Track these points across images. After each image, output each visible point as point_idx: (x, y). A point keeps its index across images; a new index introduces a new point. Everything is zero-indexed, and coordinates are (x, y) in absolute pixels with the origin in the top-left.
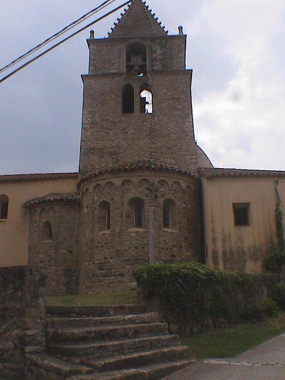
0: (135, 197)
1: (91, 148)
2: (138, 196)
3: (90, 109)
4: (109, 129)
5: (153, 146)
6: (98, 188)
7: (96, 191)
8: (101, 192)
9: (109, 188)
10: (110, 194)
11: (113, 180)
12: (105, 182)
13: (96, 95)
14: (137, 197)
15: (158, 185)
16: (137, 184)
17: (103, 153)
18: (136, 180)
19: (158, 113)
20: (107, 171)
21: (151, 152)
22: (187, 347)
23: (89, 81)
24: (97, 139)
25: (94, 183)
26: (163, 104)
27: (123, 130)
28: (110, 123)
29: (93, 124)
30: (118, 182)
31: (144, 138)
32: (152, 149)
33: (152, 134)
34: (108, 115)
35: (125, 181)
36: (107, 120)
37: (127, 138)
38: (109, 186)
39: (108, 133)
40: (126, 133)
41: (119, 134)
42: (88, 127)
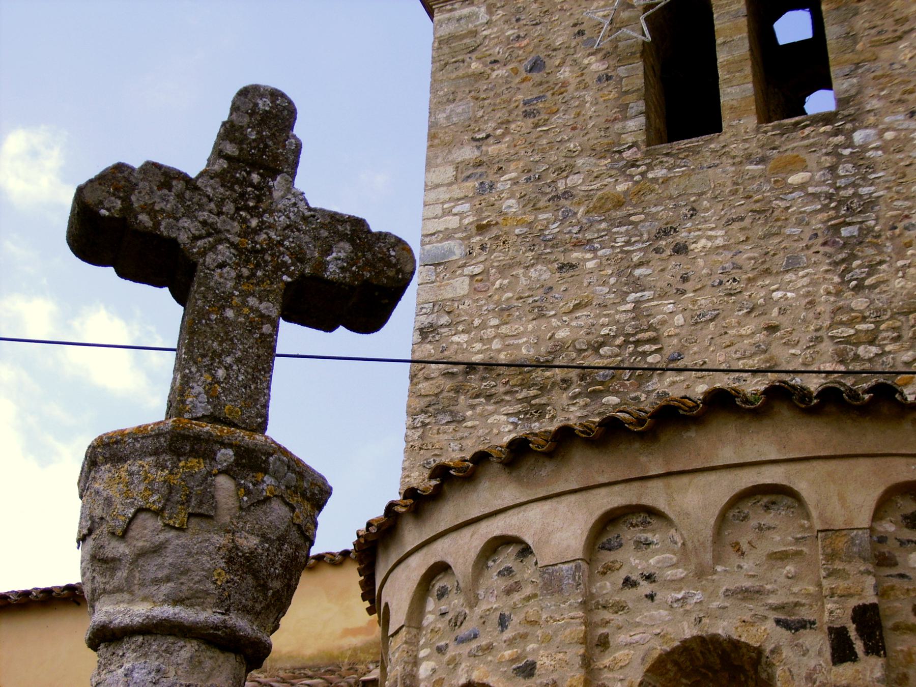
0: (701, 640)
1: (471, 367)
2: (723, 628)
3: (468, 153)
4: (578, 245)
5: (859, 303)
6: (442, 594)
7: (429, 619)
8: (457, 622)
9: (502, 584)
10: (508, 634)
11: (525, 523)
12: (471, 543)
13: (501, 72)
14: (714, 640)
15: (888, 527)
16: (708, 533)
17: (543, 389)
18: (694, 502)
19: (875, 104)
20: (481, 458)
21: (847, 340)
22: (790, 181)
23: (466, 11)
24: (505, 312)
25: (414, 561)
26: (902, 45)
27: (665, 233)
28: (581, 210)
29: (481, 229)
30: (557, 526)
31: (792, 265)
32: (850, 323)
33: (845, 232)
34: (571, 169)
35: (609, 521)
36: (568, 194)
37: (685, 279)
38: (507, 572)
39: (572, 266)
40: (681, 249)
41: (640, 264)
42: (457, 250)
